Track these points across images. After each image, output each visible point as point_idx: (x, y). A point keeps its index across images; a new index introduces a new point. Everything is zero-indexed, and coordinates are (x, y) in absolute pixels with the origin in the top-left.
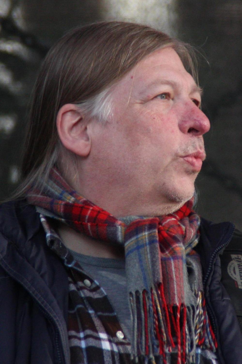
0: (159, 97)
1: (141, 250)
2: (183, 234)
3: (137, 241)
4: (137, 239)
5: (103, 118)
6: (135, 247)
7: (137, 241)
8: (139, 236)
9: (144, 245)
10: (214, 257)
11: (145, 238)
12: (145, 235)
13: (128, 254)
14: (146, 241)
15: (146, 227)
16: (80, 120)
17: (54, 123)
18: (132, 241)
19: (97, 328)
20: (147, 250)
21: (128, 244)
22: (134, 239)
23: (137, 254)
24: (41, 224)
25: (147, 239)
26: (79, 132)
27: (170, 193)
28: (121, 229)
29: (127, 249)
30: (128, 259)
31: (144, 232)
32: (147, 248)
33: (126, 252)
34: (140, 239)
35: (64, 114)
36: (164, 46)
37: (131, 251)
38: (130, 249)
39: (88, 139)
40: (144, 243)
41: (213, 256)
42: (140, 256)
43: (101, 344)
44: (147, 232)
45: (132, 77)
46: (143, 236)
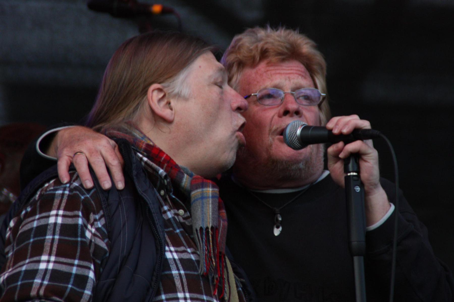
1: (205, 201)
3: (202, 193)
4: (202, 191)
5: (285, 50)
6: (200, 196)
7: (202, 193)
8: (205, 189)
11: (209, 193)
13: (194, 201)
14: (209, 195)
16: (164, 96)
18: (198, 192)
19: (153, 214)
20: (209, 201)
21: (195, 193)
22: (200, 190)
23: (201, 202)
27: (292, 174)
28: (186, 177)
29: (194, 198)
30: (193, 205)
33: (192, 200)
34: (205, 192)
35: (153, 91)
36: (205, 49)
37: (197, 200)
38: (196, 198)
39: (171, 109)
40: (208, 195)
42: (203, 203)
43: (55, 210)
46: (207, 190)
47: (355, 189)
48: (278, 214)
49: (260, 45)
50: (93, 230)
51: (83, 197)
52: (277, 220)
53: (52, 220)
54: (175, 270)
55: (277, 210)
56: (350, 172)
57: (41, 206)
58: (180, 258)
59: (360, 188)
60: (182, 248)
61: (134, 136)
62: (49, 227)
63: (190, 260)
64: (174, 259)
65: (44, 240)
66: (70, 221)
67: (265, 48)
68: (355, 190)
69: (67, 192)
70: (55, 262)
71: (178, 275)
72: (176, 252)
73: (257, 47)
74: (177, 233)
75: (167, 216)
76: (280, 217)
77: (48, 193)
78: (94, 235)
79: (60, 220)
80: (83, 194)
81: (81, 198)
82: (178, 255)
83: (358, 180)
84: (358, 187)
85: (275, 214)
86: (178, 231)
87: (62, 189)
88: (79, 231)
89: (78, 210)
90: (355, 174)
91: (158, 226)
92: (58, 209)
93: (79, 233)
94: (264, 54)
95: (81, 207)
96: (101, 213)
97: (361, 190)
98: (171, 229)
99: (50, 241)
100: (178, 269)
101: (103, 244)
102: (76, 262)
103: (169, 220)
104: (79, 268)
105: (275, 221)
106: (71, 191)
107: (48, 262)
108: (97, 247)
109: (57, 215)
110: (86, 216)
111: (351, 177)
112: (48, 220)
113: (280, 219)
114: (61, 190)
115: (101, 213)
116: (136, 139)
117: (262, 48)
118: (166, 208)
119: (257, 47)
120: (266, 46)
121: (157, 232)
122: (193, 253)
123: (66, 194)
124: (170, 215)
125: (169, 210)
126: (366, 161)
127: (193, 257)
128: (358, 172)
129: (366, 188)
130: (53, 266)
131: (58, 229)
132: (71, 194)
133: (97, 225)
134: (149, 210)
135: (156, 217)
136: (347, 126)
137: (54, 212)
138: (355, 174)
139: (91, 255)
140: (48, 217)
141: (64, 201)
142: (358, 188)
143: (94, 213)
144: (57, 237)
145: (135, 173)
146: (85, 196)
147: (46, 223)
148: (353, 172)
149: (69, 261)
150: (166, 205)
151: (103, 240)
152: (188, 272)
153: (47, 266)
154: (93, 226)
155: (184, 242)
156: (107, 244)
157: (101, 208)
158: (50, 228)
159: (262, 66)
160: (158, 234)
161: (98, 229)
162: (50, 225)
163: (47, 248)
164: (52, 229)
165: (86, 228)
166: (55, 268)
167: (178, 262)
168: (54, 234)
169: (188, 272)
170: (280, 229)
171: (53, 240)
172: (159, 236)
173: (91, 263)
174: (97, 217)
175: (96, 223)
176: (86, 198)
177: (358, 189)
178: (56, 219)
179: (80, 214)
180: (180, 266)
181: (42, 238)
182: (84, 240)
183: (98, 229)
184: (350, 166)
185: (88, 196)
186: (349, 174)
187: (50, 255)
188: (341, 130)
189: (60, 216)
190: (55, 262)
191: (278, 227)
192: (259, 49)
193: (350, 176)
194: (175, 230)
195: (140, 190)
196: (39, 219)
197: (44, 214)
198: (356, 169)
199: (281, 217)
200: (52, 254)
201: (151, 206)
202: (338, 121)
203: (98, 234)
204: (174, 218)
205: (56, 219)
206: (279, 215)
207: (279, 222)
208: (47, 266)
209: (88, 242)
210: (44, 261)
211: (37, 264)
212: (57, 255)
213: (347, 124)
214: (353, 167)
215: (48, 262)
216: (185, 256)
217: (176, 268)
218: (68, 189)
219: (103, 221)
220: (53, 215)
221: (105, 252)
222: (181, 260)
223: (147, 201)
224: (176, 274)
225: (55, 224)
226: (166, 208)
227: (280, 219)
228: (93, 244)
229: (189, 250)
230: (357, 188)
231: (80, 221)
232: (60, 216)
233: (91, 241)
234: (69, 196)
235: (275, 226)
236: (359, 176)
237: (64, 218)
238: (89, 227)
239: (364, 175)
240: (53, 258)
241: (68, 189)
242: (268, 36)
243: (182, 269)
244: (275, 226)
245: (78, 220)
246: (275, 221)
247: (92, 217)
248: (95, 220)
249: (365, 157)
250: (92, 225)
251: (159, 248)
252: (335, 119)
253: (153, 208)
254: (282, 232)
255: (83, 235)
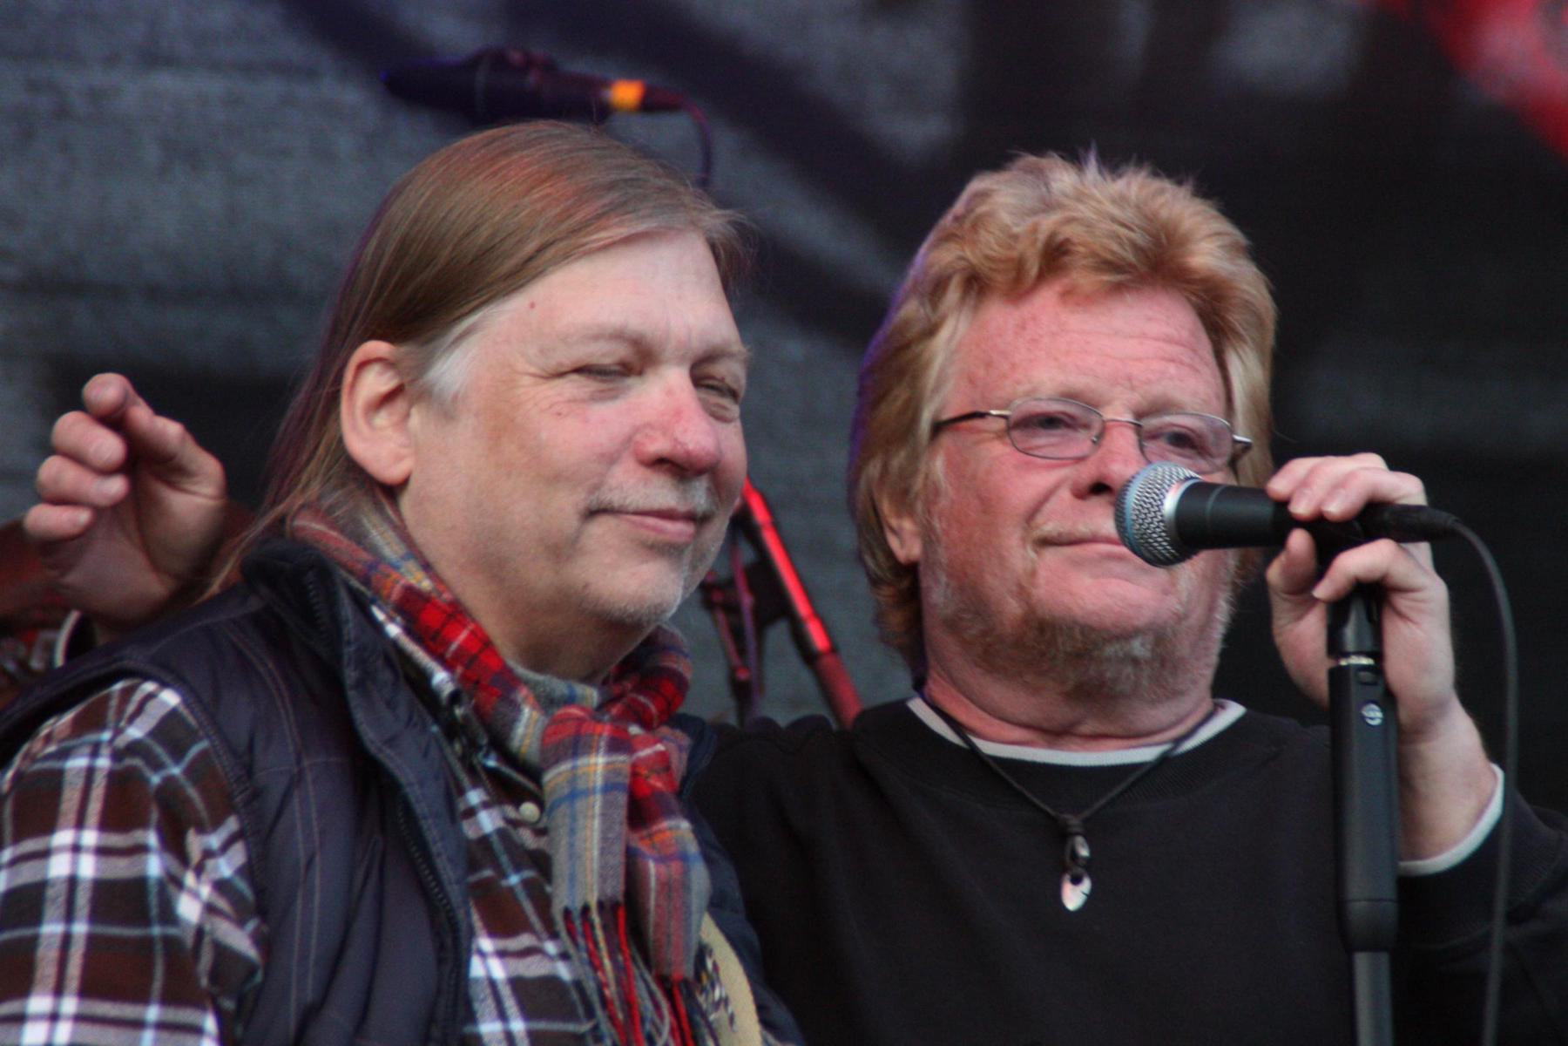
0: (666, 466)
2: (1031, 449)
3: (573, 778)
4: (574, 768)
9: (589, 792)
10: (596, 965)
11: (595, 771)
12: (596, 764)
14: (595, 782)
15: (602, 744)
17: (335, 369)
24: (394, 643)
25: (598, 776)
26: (395, 418)
27: (1108, 675)
31: (594, 754)
32: (594, 802)
35: (363, 365)
41: (430, 874)
43: (66, 827)
44: (603, 756)
45: (532, 306)
46: (589, 765)
47: (1365, 713)
48: (1077, 834)
49: (1048, 223)
50: (206, 891)
51: (156, 779)
52: (1074, 855)
53: (59, 867)
54: (493, 1021)
55: (1074, 822)
56: (1347, 655)
57: (18, 816)
58: (515, 974)
59: (1383, 710)
60: (525, 940)
61: (373, 549)
62: (50, 893)
63: (552, 982)
64: (492, 983)
65: (33, 942)
66: (120, 868)
67: (1061, 237)
68: (1363, 718)
69: (104, 762)
70: (79, 1018)
71: (501, 1036)
72: (502, 954)
73: (1035, 230)
74: (511, 889)
75: (478, 826)
76: (1083, 846)
77: (38, 766)
78: (210, 909)
79: (88, 867)
80: (157, 766)
81: (146, 781)
82: (505, 967)
83: (1374, 684)
84: (1374, 707)
85: (1063, 836)
86: (514, 880)
87: (87, 750)
88: (153, 900)
89: (143, 824)
90: (1365, 661)
91: (442, 863)
92: (80, 824)
93: (154, 912)
94: (1055, 256)
95: (155, 816)
96: (232, 824)
97: (1385, 720)
98: (488, 873)
99: (57, 943)
100: (503, 1016)
101: (240, 940)
102: (153, 1013)
103: (484, 840)
104: (165, 1035)
105: (1068, 859)
106: (117, 756)
107: (54, 1017)
108: (223, 953)
109: (76, 849)
110: (174, 845)
111: (1352, 674)
112: (46, 868)
113: (1084, 852)
114: (82, 755)
115: (232, 824)
116: (379, 559)
117: (1052, 236)
118: (475, 797)
119: (1035, 230)
120: (1068, 232)
121: (439, 883)
122: (564, 956)
123: (101, 769)
124: (488, 822)
125: (486, 805)
126: (1402, 616)
127: (564, 971)
128: (1378, 655)
129: (1404, 715)
130: (74, 1033)
131: (83, 899)
132: (119, 767)
133: (216, 868)
134: (408, 808)
135: (432, 831)
136: (1342, 491)
137: (63, 837)
138: (1365, 661)
139: (204, 982)
140: (45, 854)
141: (98, 792)
142: (1373, 710)
143: (201, 830)
144: (80, 928)
145: (350, 675)
146: (164, 773)
147: (38, 878)
148: (1359, 653)
149: (128, 1011)
150: (475, 786)
151: (240, 923)
152: (542, 1025)
153: (51, 1032)
154: (204, 877)
155: (534, 919)
156: (258, 940)
157: (229, 809)
158: (55, 895)
159: (1046, 300)
160: (442, 889)
161: (221, 886)
162: (53, 885)
163: (46, 968)
164: (62, 899)
165: (179, 885)
166: (79, 1040)
167: (506, 992)
168: (69, 917)
169: (542, 1025)
170: (1086, 885)
171: (67, 939)
172: (446, 896)
173: (203, 1008)
174: (215, 841)
175: (210, 863)
176: (169, 780)
177: (1374, 715)
178: (75, 864)
179: (152, 839)
180: (510, 1004)
181: (26, 932)
182: (172, 931)
183: (221, 886)
184: (1349, 632)
185: (176, 771)
186: (1343, 663)
187: (58, 992)
188: (1322, 502)
189: (87, 850)
190: (79, 1018)
191: (1076, 881)
192: (1042, 237)
193: (1348, 667)
194: (505, 876)
195: (370, 735)
196: (15, 862)
197: (30, 845)
198: (1368, 645)
199: (1085, 845)
200: (67, 991)
201: (414, 793)
202: (1312, 472)
203: (222, 904)
204: (500, 832)
205: (75, 864)
206: (1080, 840)
207: (1081, 862)
208: (51, 1032)
209: (189, 941)
210: (38, 1017)
211: (12, 1029)
212: (85, 992)
213: (1339, 485)
214: (1358, 635)
215: (54, 1017)
216: (533, 968)
217: (494, 1013)
218: (105, 751)
219: (238, 855)
220: (60, 849)
221: (251, 969)
222: (517, 983)
223: (397, 773)
224: (493, 1034)
225: (73, 882)
226: (475, 797)
227: (1084, 852)
228: (207, 939)
229: (551, 947)
230: (1369, 710)
231: (154, 866)
232: (87, 850)
233: (200, 932)
234: (112, 776)
235: (1067, 878)
236: (1378, 670)
237: (104, 859)
238: (189, 879)
239: (1398, 668)
240: (70, 1005)
241: (105, 751)
242: (1080, 197)
243: (518, 1014)
244: (1067, 878)
245: (145, 863)
246: (1068, 859)
247: (195, 843)
248: (208, 854)
249: (1402, 602)
250: (199, 870)
251: (449, 941)
252: (1300, 467)
253: (422, 795)
254: (1091, 898)
255: (168, 915)
